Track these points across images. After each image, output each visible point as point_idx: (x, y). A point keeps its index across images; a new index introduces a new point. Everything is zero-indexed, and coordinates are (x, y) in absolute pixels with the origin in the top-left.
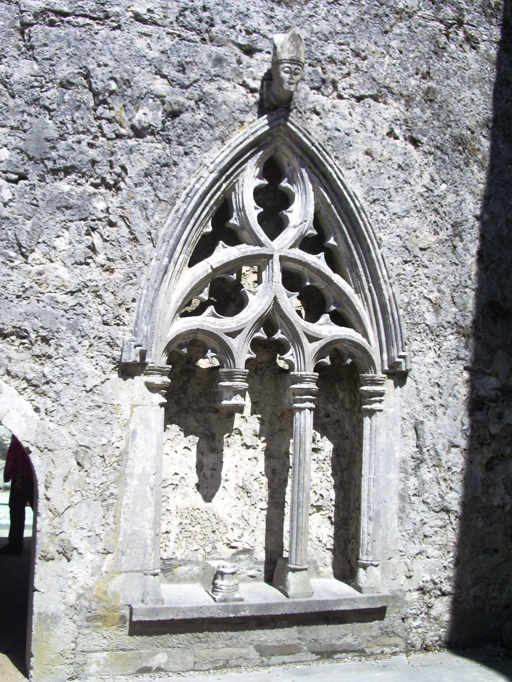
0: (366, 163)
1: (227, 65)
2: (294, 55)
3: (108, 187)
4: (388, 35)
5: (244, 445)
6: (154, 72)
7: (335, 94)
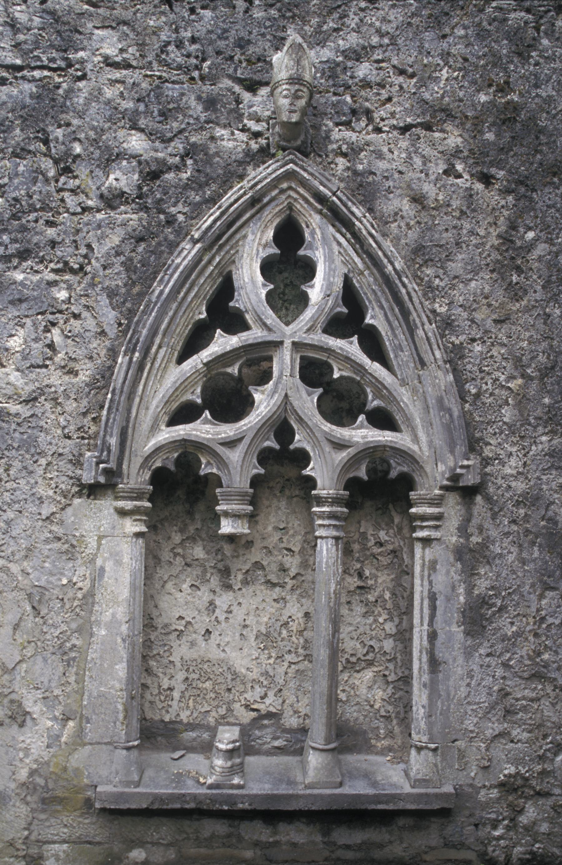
0: (412, 213)
1: (222, 106)
2: (293, 72)
3: (73, 271)
4: (446, 40)
5: (268, 582)
6: (128, 126)
7: (370, 128)
